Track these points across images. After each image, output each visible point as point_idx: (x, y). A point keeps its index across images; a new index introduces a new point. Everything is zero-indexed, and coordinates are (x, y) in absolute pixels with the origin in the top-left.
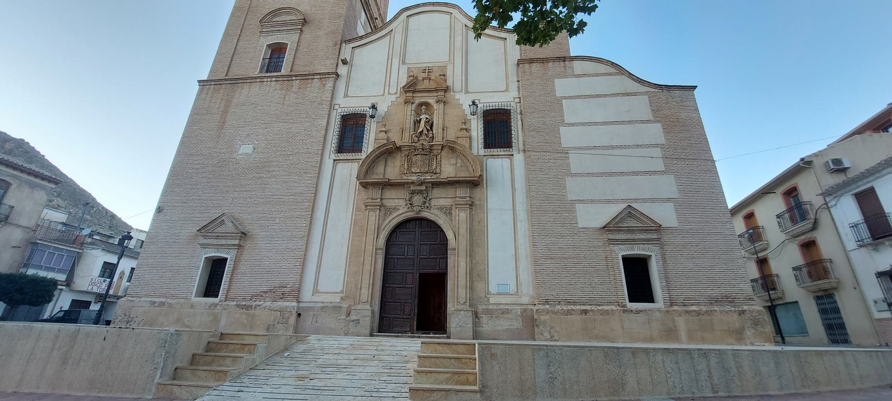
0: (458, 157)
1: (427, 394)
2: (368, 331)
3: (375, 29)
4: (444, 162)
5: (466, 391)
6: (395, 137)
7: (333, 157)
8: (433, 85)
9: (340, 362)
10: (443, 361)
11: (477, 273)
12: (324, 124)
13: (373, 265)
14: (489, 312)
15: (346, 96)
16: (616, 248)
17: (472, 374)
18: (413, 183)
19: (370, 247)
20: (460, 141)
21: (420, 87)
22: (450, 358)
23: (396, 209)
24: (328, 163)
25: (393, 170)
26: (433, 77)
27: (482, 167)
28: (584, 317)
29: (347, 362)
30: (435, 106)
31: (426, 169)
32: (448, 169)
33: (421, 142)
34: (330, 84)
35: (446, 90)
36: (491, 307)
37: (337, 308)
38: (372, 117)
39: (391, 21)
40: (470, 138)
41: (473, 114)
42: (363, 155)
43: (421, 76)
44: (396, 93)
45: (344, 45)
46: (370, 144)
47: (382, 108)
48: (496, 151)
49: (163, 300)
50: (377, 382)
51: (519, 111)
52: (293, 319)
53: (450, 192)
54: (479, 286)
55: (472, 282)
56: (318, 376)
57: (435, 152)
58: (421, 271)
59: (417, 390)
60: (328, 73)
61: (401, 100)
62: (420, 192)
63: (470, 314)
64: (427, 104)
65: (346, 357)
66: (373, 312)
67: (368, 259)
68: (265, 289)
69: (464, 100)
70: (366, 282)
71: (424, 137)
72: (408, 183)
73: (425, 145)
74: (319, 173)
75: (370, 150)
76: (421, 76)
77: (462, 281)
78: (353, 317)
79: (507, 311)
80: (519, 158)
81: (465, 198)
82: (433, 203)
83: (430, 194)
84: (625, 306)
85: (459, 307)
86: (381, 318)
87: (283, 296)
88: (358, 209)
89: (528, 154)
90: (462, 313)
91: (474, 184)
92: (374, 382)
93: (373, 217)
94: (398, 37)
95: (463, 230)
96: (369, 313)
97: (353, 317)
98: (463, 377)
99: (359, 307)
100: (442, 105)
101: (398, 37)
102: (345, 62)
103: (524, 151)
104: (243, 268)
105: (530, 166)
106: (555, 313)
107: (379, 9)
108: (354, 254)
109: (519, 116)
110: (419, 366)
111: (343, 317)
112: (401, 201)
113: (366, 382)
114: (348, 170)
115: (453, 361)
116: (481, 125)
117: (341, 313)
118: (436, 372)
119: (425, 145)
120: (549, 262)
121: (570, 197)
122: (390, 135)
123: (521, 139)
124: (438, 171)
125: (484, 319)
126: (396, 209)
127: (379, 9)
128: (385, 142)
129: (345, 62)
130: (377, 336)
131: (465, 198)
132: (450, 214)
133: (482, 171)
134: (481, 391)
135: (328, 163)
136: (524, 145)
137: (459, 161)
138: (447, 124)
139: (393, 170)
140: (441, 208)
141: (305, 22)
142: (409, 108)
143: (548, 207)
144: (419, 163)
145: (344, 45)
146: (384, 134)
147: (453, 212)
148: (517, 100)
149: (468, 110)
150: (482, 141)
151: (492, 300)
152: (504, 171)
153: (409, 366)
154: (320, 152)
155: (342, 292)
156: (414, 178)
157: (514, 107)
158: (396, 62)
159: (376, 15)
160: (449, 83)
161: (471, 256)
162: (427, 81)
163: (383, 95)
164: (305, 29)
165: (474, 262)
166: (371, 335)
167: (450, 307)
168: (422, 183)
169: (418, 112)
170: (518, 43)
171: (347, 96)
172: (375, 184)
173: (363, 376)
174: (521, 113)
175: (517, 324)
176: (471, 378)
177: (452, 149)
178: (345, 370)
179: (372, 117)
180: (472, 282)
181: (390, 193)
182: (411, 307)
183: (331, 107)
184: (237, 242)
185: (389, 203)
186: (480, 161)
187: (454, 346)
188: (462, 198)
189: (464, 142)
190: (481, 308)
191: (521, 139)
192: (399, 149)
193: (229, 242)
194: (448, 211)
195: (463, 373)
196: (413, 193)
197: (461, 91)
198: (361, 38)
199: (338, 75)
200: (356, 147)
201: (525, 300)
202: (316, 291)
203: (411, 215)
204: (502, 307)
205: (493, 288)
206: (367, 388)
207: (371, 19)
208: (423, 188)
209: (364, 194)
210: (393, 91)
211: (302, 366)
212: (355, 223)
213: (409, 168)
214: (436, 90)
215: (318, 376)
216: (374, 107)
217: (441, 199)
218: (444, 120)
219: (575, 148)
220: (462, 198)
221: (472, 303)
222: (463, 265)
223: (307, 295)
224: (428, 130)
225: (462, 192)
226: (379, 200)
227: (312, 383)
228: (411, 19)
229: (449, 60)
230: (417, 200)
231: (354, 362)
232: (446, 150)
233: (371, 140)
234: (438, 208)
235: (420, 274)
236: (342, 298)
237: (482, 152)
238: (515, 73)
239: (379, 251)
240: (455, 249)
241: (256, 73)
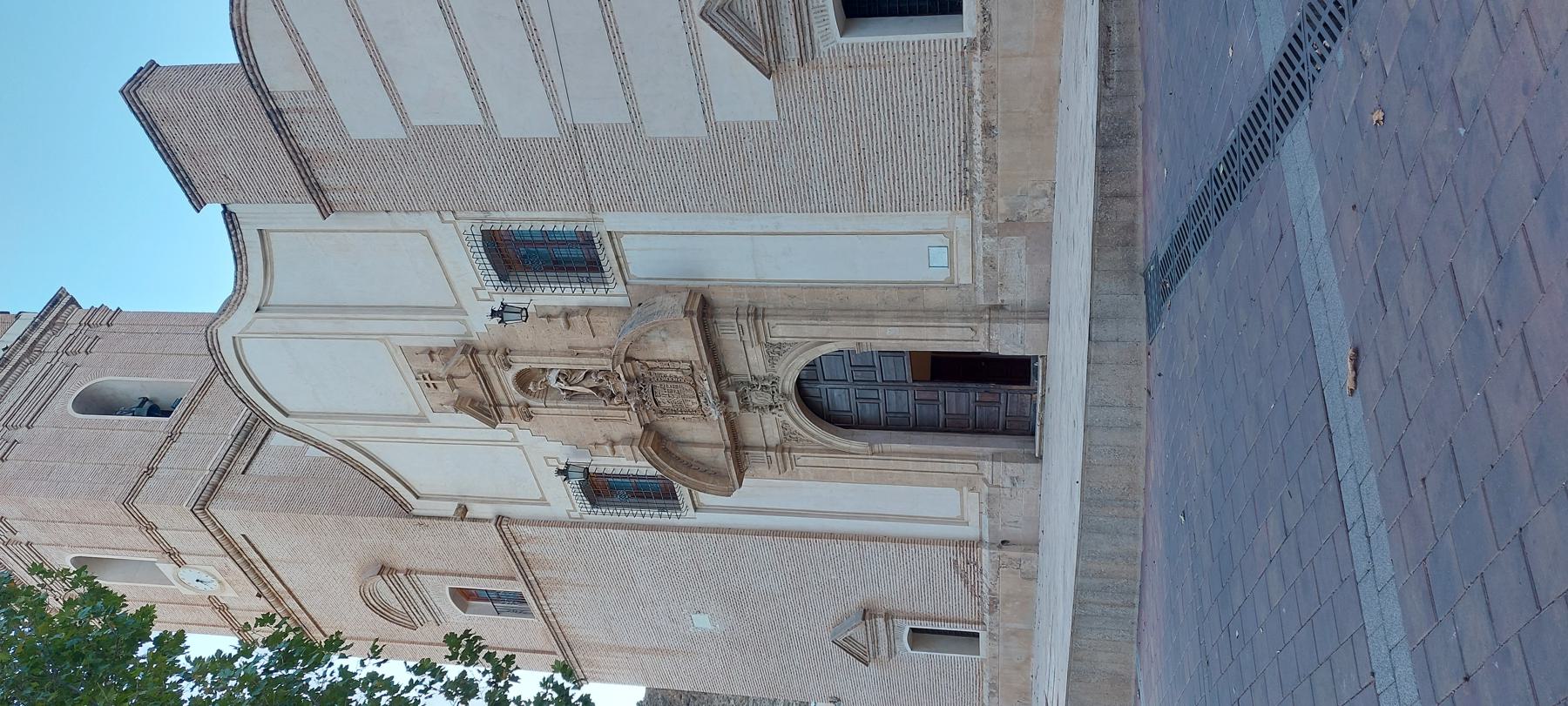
2: (1033, 467)
4: (660, 354)
11: (910, 302)
14: (991, 289)
16: (822, 48)
28: (999, 131)
30: (518, 368)
47: (562, 454)
49: (986, 685)
52: (1014, 554)
54: (934, 298)
60: (503, 536)
62: (743, 398)
68: (961, 584)
79: (990, 263)
81: (741, 328)
82: (760, 371)
83: (742, 379)
84: (972, 44)
87: (973, 563)
90: (993, 338)
91: (704, 311)
102: (463, 511)
104: (925, 608)
105: (623, 204)
106: (992, 186)
108: (880, 476)
120: (872, 185)
121: (698, 130)
125: (1004, 297)
126: (784, 426)
131: (741, 328)
141: (384, 570)
143: (728, 171)
147: (775, 341)
152: (651, 244)
157: (471, 224)
158: (422, 432)
164: (402, 565)
168: (724, 399)
171: (544, 499)
184: (881, 621)
190: (982, 301)
193: (883, 635)
197: (463, 322)
201: (962, 223)
203: (793, 406)
208: (732, 394)
219: (555, 107)
223: (970, 532)
225: (730, 335)
228: (288, 407)
238: (369, 216)
241: (537, 622)
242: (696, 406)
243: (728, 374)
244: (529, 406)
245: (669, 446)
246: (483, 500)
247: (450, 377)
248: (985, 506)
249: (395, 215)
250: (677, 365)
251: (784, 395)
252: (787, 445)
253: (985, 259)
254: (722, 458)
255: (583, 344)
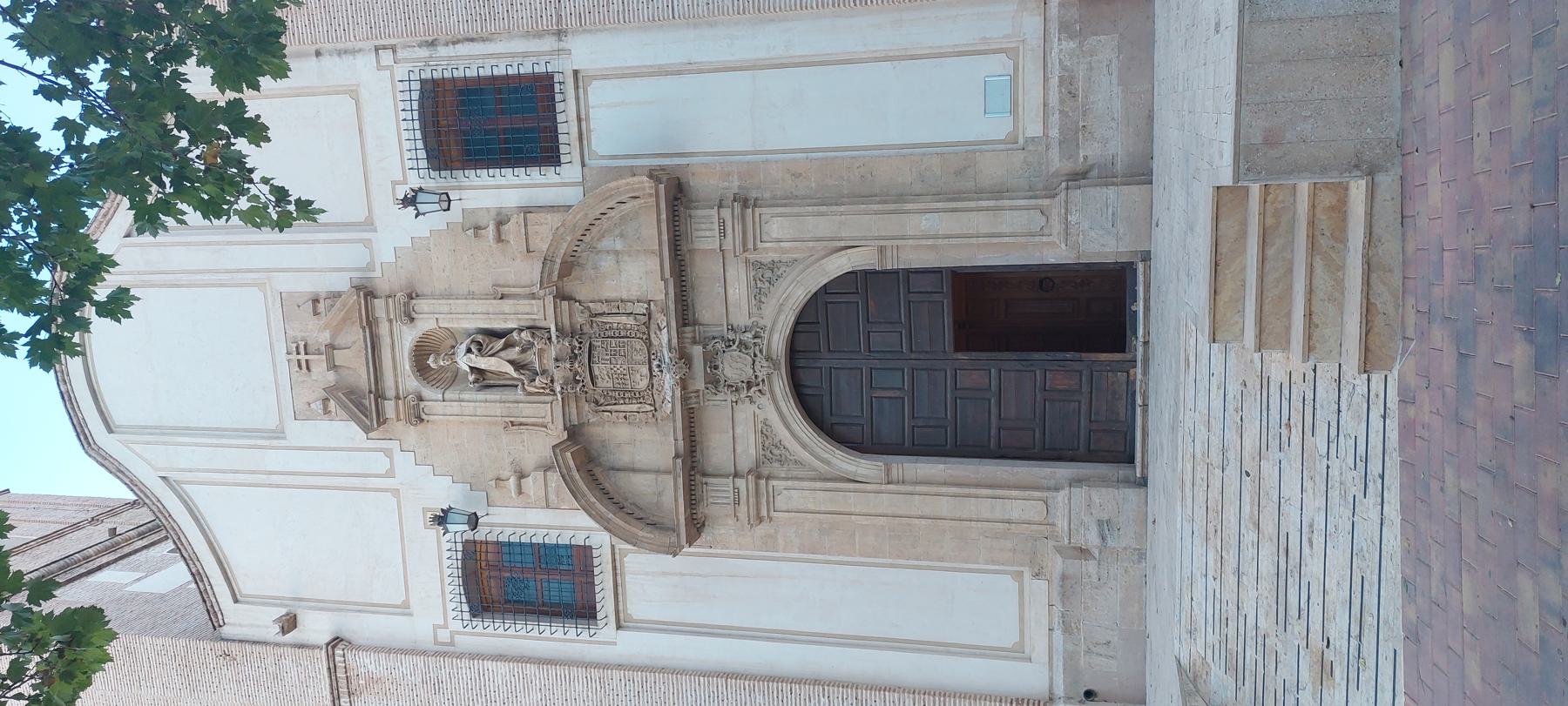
0: (592, 248)
1: (1379, 322)
2: (1132, 494)
3: (158, 530)
5: (1370, 215)
6: (539, 445)
7: (606, 630)
8: (355, 336)
9: (1267, 567)
10: (1270, 278)
11: (954, 179)
12: (503, 668)
13: (936, 488)
14: (1071, 138)
15: (404, 609)
17: (1313, 196)
18: (683, 383)
19: (885, 502)
20: (542, 244)
21: (360, 376)
22: (1263, 260)
23: (765, 432)
24: (629, 645)
25: (643, 446)
26: (325, 337)
27: (619, 173)
29: (1267, 550)
30: (425, 325)
31: (638, 344)
32: (632, 276)
33: (549, 364)
34: (364, 664)
35: (367, 292)
36: (1054, 133)
37: (1067, 587)
38: (474, 521)
39: (132, 483)
40: (526, 210)
41: (446, 202)
42: (601, 540)
43: (321, 374)
44: (388, 453)
45: (226, 631)
46: (562, 521)
47: (444, 492)
48: (567, 128)
50: (1335, 464)
51: (424, 53)
53: (705, 270)
54: (992, 170)
55: (979, 193)
56: (1316, 627)
57: (580, 319)
58: (949, 346)
59: (1366, 351)
60: (332, 670)
61: (411, 434)
62: (711, 362)
63: (1076, 195)
64: (421, 354)
65: (1249, 553)
66: (1076, 482)
67: (918, 505)
69: (399, 233)
70: (982, 506)
71: (532, 357)
72: (685, 400)
73: (562, 354)
74: (663, 670)
75: (582, 519)
76: (321, 374)
77: (978, 222)
78: (1092, 539)
79: (1068, 81)
80: (583, 53)
81: (722, 223)
82: (741, 319)
83: (714, 331)
85: (1057, 226)
86: (1091, 456)
88: (769, 543)
89: (570, 23)
90: (1072, 219)
91: (677, 195)
92: (1334, 472)
93: (791, 496)
94: (184, 457)
95: (822, 225)
96: (1079, 493)
97: (1092, 539)
98: (1324, 221)
99: (1062, 524)
100: (421, 305)
101: (184, 457)
102: (289, 623)
103: (560, 34)
107: (76, 527)
108: (903, 545)
109: (443, 51)
110: (1285, 346)
111: (1091, 567)
112: (740, 416)
113: (1334, 494)
114: (645, 580)
115: (1270, 252)
116: (482, 177)
117: (1073, 570)
118: (1309, 301)
119: (562, 354)
122: (529, 461)
123: (518, 46)
124: (641, 308)
125: (1090, 151)
126: (765, 432)
127: (76, 527)
128: (555, 478)
129: (289, 623)
130: (1144, 466)
131: (722, 223)
132: (773, 267)
133: (633, 172)
134: (1371, 173)
135: (629, 645)
136: (539, 35)
137: (607, 243)
138: (486, 285)
139: (643, 446)
140: (758, 295)
142: (439, 407)
144: (621, 366)
145: (226, 631)
146: (528, 483)
147: (767, 258)
148: (386, 58)
149: (435, 220)
150: (534, 171)
151: (1034, 129)
153: (1277, 374)
154: (595, 673)
155: (1018, 576)
156: (668, 380)
157: (416, 64)
158: (275, 459)
159: (99, 534)
160: (342, 283)
161: (901, 198)
162: (340, 357)
163: (395, 492)
165: (918, 188)
166: (1143, 483)
167: (1055, 253)
168: (684, 357)
169: (451, 378)
170: (281, 72)
172: (693, 498)
173: (1314, 502)
174: (432, 44)
175: (1106, 47)
176: (1327, 199)
177: (569, 266)
178: (1294, 553)
179: (474, 521)
180: (979, 193)
181: (718, 451)
182: (1057, 372)
183: (444, 652)
185: (748, 451)
186: (599, 179)
187: (1223, 250)
188: (723, 233)
189: (544, 231)
190: (1057, 162)
191: (518, 46)
192: (574, 433)
194: (765, 275)
195: (1312, 223)
196: (714, 382)
197: (367, 243)
198: (198, 576)
199: (336, 641)
200: (578, 561)
201: (1032, 25)
202: (1017, 652)
203: (781, 385)
204: (1054, 99)
205: (996, 127)
206: (1356, 490)
207: (117, 549)
208: (697, 351)
209: (723, 529)
210: (380, 463)
211: (1286, 672)
212: (811, 549)
213: (637, 396)
214: (371, 323)
215: (1316, 627)
216: (441, 519)
217: (728, 296)
218: (471, 296)
220: (723, 233)
221: (1043, 188)
222: (926, 223)
224: (507, 346)
225: (705, 234)
226: (741, 483)
227: (1339, 642)
228: (118, 416)
229: (260, 285)
230: (734, 367)
231: (1269, 527)
232: (571, 286)
233: (549, 518)
234: (757, 303)
235: (957, 349)
236: (1037, 575)
237: (570, 171)
239: (894, 472)
240: (882, 250)
242: (643, 384)
243: (695, 323)
244: (421, 399)
245: (597, 471)
246: (322, 605)
247: (331, 347)
248: (1058, 608)
249: (326, 61)
250: (629, 308)
251: (768, 358)
252: (765, 471)
253: (1061, 79)
254: (668, 494)
255: (511, 279)
